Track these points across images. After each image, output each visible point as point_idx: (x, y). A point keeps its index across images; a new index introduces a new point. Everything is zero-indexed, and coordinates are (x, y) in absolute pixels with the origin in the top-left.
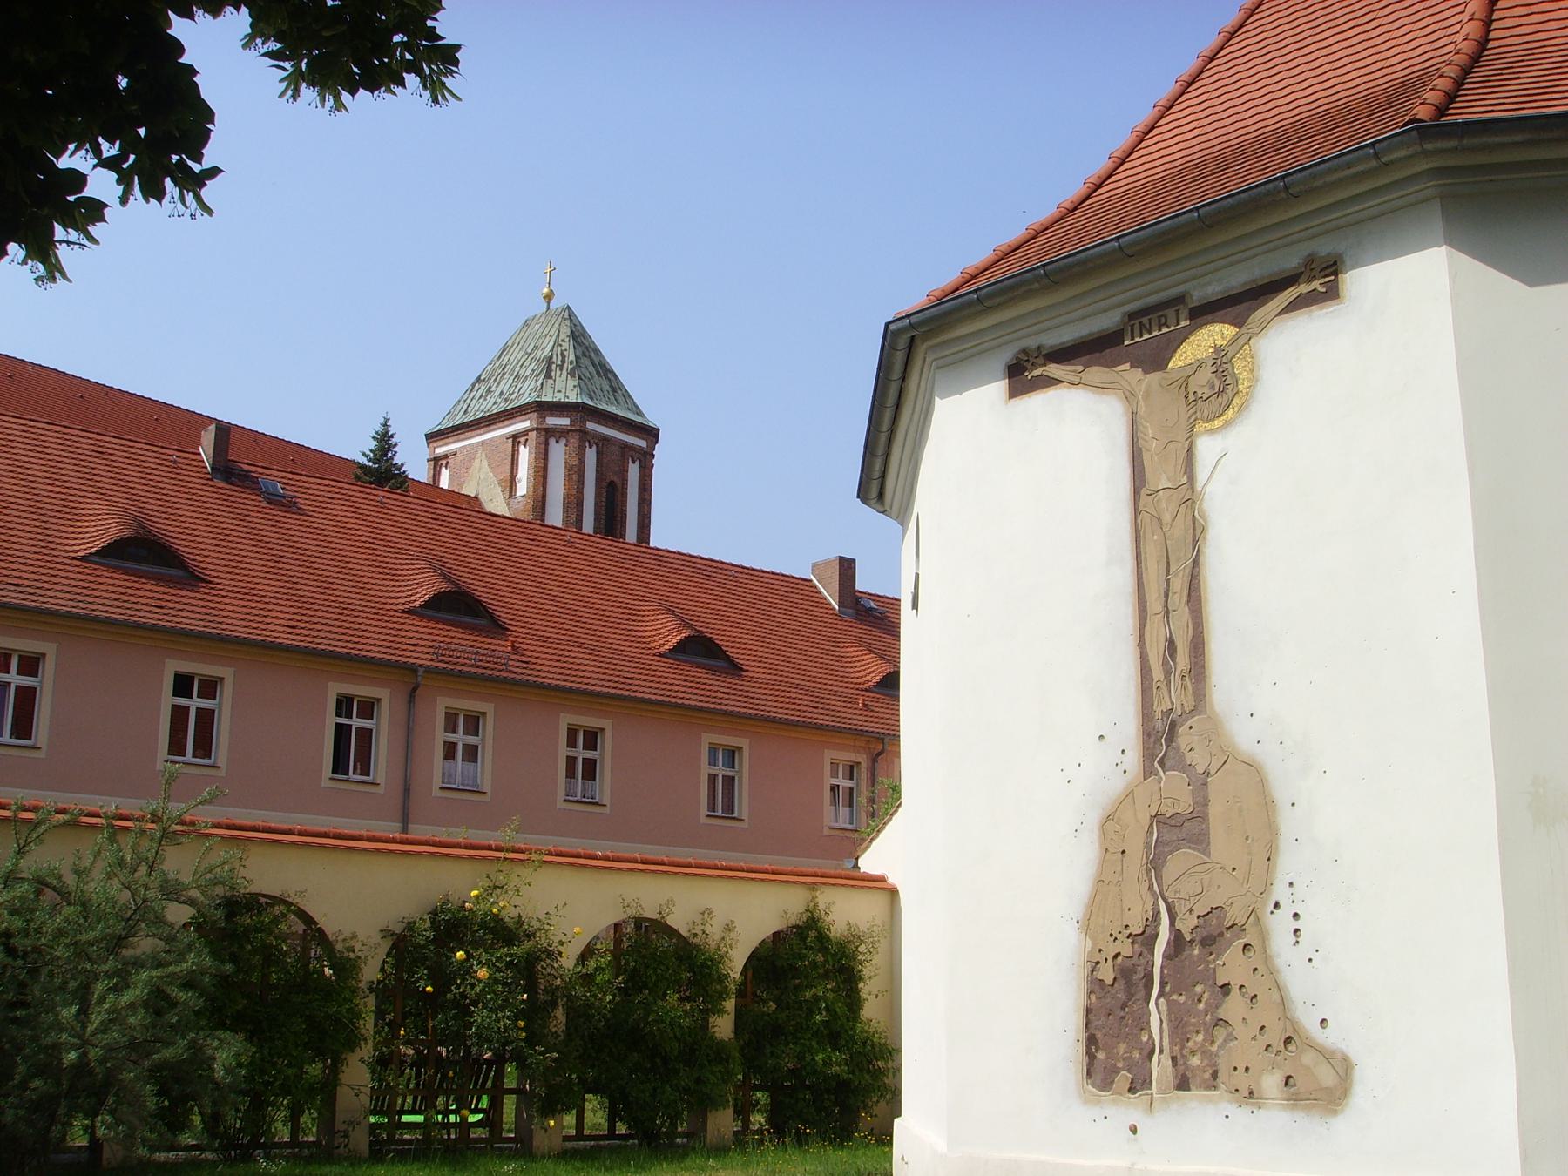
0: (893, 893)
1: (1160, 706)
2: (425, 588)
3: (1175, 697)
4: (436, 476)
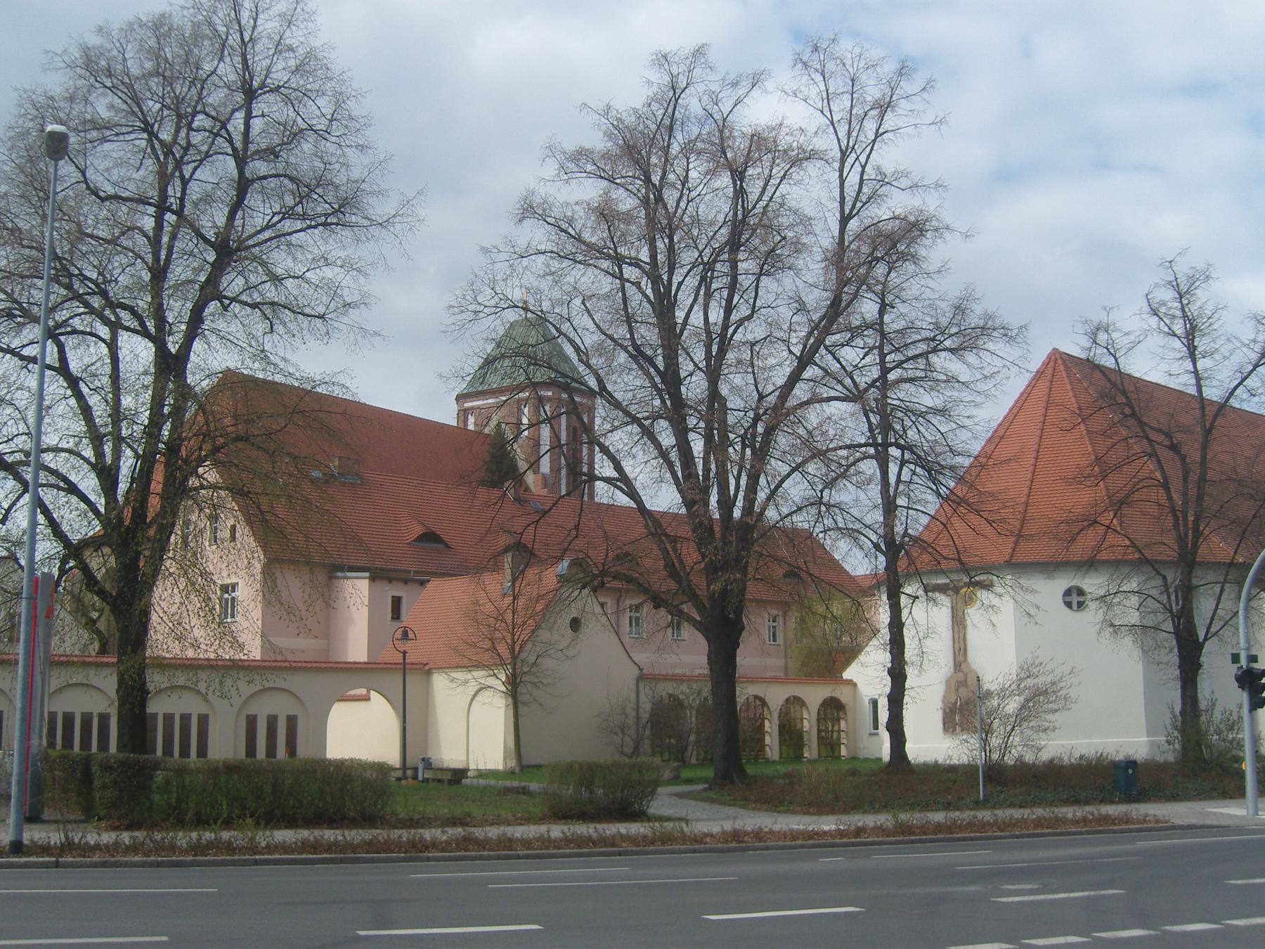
0: (855, 685)
1: (958, 659)
2: (418, 530)
3: (961, 658)
4: (466, 422)
